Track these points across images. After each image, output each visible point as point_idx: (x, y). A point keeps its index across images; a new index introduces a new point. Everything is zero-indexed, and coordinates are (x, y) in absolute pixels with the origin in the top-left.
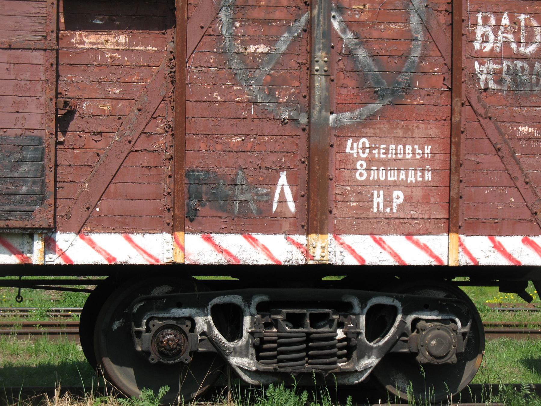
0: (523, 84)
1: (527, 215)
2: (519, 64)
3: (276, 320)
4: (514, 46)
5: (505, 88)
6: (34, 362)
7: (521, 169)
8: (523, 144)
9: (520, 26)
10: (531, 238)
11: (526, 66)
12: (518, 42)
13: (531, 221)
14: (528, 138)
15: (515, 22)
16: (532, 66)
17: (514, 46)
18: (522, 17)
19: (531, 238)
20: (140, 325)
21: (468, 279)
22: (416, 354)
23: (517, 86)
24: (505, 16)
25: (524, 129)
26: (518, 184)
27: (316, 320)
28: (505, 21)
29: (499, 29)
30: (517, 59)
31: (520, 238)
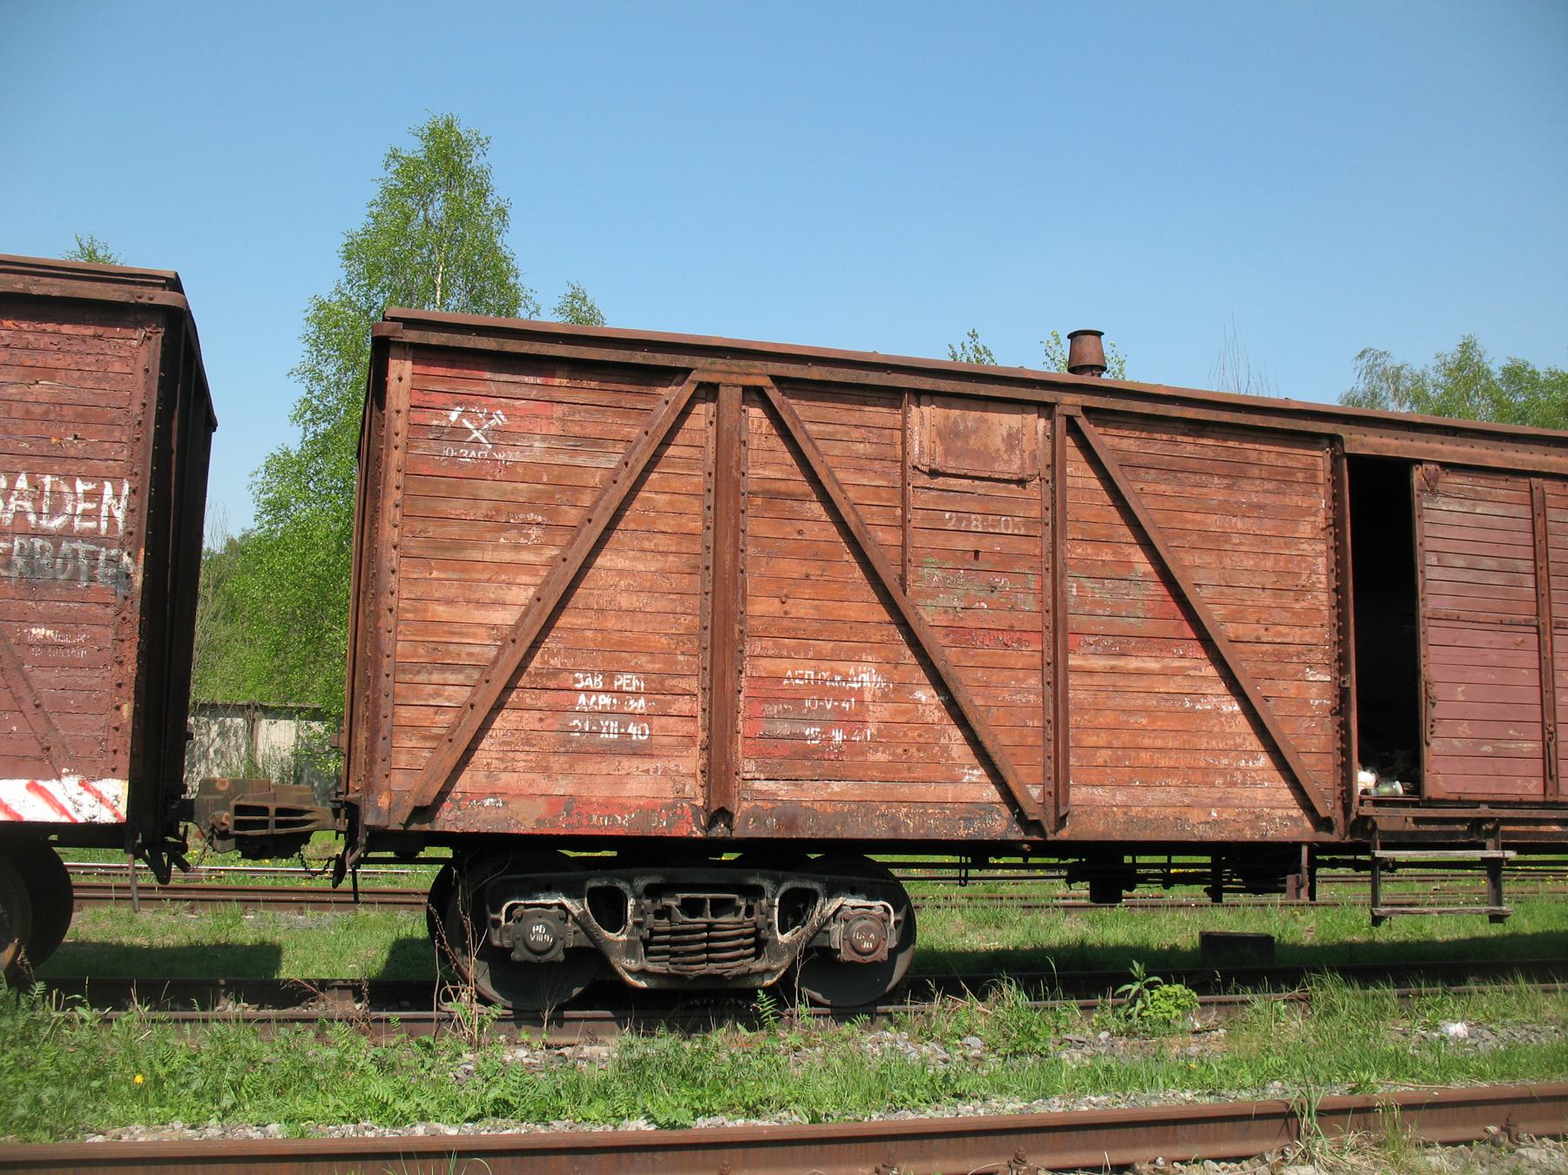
0: (41, 567)
1: (37, 751)
2: (38, 543)
3: (669, 908)
4: (32, 518)
5: (15, 574)
6: (171, 940)
7: (29, 686)
8: (37, 652)
9: (42, 491)
10: (40, 783)
11: (48, 545)
12: (39, 513)
13: (40, 759)
14: (45, 644)
15: (35, 485)
16: (57, 546)
17: (32, 518)
18: (48, 480)
19: (40, 783)
20: (498, 911)
21: (390, 854)
22: (511, 950)
23: (33, 572)
24: (23, 477)
25: (39, 632)
26: (23, 707)
27: (720, 907)
28: (22, 483)
29: (10, 495)
30: (35, 536)
31: (25, 782)
